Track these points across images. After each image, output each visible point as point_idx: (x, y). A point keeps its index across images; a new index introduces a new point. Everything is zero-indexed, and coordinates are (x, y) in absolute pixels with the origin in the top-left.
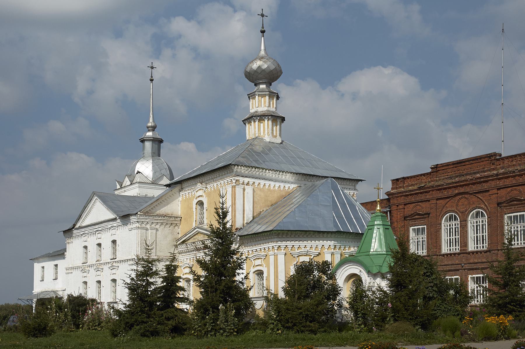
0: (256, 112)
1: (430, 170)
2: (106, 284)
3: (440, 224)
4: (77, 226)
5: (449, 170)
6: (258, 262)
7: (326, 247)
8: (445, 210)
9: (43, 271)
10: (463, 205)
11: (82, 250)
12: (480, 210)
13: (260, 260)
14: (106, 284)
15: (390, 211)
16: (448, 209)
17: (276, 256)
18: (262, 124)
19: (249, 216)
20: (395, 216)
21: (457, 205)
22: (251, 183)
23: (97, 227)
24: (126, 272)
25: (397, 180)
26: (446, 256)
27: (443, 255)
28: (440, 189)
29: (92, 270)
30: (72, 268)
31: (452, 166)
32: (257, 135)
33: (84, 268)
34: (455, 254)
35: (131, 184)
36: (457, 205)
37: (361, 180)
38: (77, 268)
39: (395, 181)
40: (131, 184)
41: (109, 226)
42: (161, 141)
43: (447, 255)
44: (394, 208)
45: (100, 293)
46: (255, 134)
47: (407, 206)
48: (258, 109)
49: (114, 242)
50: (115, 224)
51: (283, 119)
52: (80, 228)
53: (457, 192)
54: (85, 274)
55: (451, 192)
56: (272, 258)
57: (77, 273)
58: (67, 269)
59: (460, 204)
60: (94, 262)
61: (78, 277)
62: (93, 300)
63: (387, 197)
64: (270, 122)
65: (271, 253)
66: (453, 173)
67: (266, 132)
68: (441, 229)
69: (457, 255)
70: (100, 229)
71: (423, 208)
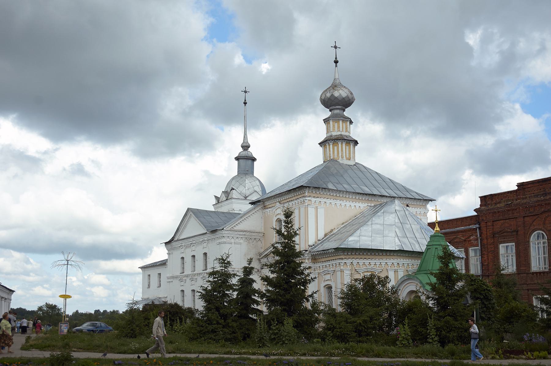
0: (331, 136)
1: (516, 188)
2: (188, 293)
3: (529, 242)
4: (176, 239)
6: (328, 277)
7: (390, 264)
8: (532, 228)
9: (149, 279)
11: (180, 260)
12: (541, 232)
13: (329, 275)
14: (188, 293)
15: (480, 228)
16: (535, 227)
17: (342, 271)
18: (336, 148)
19: (321, 235)
20: (484, 233)
21: (544, 223)
23: (191, 240)
24: (203, 283)
25: (485, 197)
26: (535, 275)
27: (533, 273)
29: (188, 280)
30: (173, 277)
32: (332, 158)
33: (181, 278)
34: (544, 273)
35: (227, 200)
36: (544, 223)
37: (431, 200)
38: (176, 277)
39: (483, 199)
40: (227, 200)
41: (201, 240)
42: (347, 103)
43: (536, 273)
44: (483, 225)
45: (183, 301)
46: (330, 157)
47: (495, 223)
48: (332, 133)
49: (205, 254)
50: (205, 238)
51: (356, 143)
52: (178, 240)
54: (182, 283)
57: (176, 282)
58: (168, 278)
60: (190, 273)
61: (177, 286)
62: (190, 309)
63: (476, 214)
64: (344, 145)
65: (338, 269)
66: (538, 191)
67: (340, 154)
68: (529, 246)
69: (546, 274)
70: (194, 242)
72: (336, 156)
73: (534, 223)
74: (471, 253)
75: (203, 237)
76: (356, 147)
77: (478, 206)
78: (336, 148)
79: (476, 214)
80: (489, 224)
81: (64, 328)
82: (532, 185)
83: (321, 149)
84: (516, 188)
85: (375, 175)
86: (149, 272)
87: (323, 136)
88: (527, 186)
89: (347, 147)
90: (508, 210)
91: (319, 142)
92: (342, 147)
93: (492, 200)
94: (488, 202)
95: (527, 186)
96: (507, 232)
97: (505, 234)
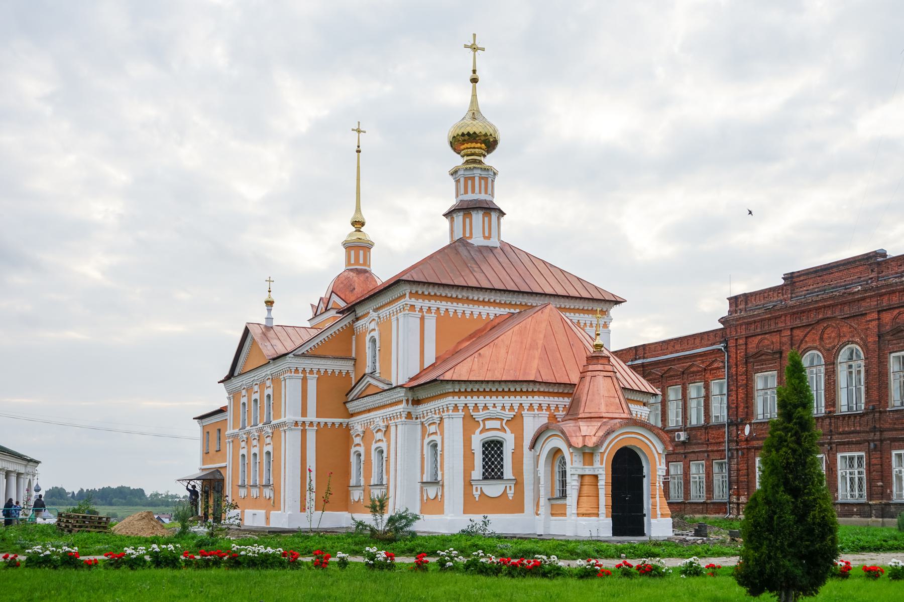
1: (782, 282)
4: (236, 374)
5: (811, 282)
7: (526, 406)
8: (803, 346)
10: (830, 338)
16: (809, 345)
20: (733, 355)
21: (821, 339)
22: (433, 310)
23: (252, 374)
28: (797, 312)
31: (813, 275)
36: (821, 339)
37: (617, 302)
39: (734, 301)
43: (844, 416)
44: (732, 343)
47: (750, 340)
53: (820, 316)
55: (813, 317)
56: (393, 429)
59: (826, 336)
63: (722, 326)
71: (773, 343)
72: (467, 235)
73: (807, 339)
74: (715, 388)
75: (265, 369)
76: (503, 220)
77: (726, 314)
78: (468, 221)
79: (722, 326)
80: (741, 342)
81: (676, 520)
82: (805, 277)
83: (446, 222)
84: (782, 282)
85: (541, 266)
86: (207, 421)
87: (451, 202)
88: (798, 279)
89: (486, 219)
90: (769, 319)
91: (445, 210)
92: (477, 217)
93: (746, 304)
94: (740, 307)
95: (798, 279)
96: (766, 354)
97: (763, 357)
